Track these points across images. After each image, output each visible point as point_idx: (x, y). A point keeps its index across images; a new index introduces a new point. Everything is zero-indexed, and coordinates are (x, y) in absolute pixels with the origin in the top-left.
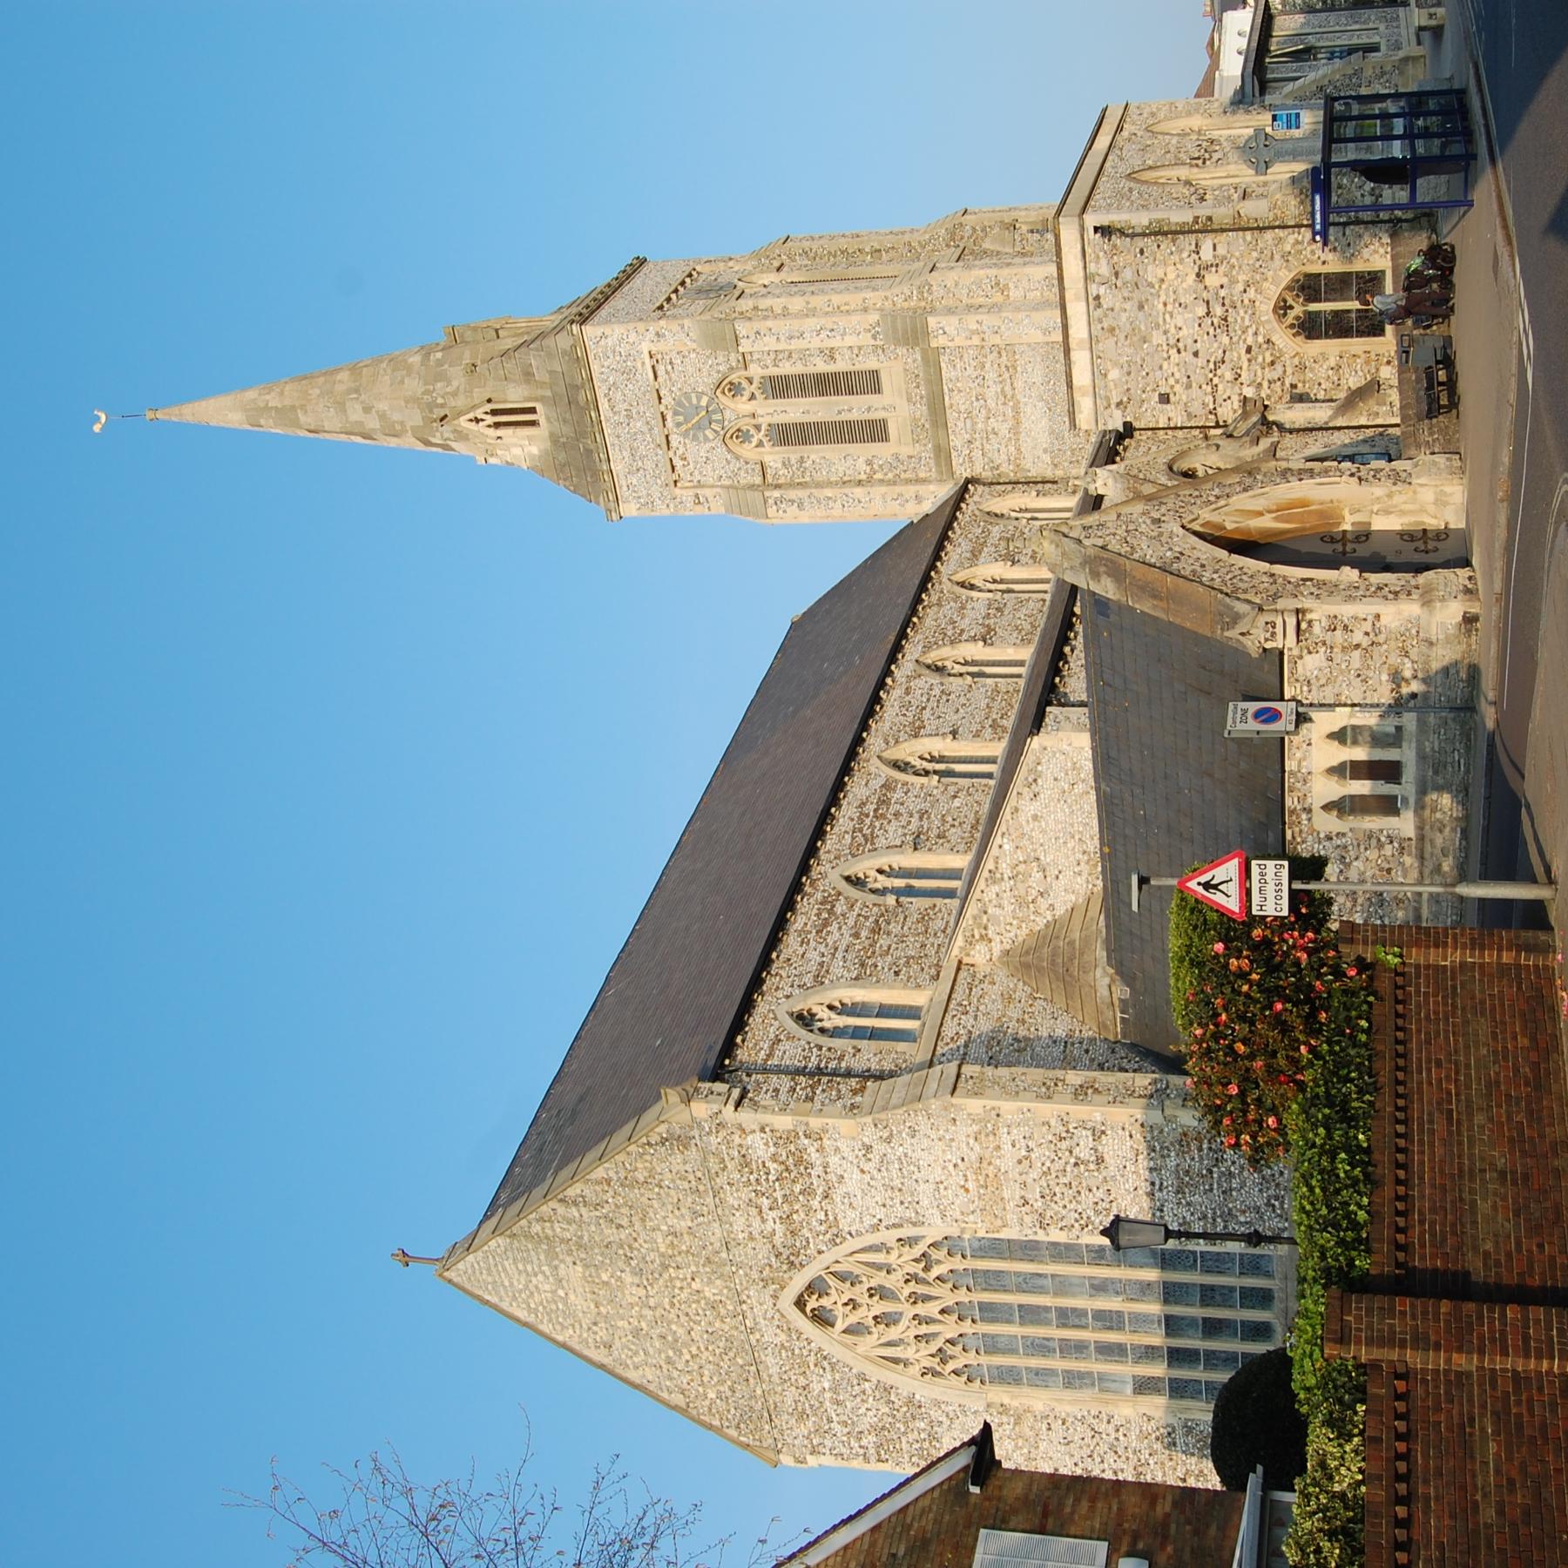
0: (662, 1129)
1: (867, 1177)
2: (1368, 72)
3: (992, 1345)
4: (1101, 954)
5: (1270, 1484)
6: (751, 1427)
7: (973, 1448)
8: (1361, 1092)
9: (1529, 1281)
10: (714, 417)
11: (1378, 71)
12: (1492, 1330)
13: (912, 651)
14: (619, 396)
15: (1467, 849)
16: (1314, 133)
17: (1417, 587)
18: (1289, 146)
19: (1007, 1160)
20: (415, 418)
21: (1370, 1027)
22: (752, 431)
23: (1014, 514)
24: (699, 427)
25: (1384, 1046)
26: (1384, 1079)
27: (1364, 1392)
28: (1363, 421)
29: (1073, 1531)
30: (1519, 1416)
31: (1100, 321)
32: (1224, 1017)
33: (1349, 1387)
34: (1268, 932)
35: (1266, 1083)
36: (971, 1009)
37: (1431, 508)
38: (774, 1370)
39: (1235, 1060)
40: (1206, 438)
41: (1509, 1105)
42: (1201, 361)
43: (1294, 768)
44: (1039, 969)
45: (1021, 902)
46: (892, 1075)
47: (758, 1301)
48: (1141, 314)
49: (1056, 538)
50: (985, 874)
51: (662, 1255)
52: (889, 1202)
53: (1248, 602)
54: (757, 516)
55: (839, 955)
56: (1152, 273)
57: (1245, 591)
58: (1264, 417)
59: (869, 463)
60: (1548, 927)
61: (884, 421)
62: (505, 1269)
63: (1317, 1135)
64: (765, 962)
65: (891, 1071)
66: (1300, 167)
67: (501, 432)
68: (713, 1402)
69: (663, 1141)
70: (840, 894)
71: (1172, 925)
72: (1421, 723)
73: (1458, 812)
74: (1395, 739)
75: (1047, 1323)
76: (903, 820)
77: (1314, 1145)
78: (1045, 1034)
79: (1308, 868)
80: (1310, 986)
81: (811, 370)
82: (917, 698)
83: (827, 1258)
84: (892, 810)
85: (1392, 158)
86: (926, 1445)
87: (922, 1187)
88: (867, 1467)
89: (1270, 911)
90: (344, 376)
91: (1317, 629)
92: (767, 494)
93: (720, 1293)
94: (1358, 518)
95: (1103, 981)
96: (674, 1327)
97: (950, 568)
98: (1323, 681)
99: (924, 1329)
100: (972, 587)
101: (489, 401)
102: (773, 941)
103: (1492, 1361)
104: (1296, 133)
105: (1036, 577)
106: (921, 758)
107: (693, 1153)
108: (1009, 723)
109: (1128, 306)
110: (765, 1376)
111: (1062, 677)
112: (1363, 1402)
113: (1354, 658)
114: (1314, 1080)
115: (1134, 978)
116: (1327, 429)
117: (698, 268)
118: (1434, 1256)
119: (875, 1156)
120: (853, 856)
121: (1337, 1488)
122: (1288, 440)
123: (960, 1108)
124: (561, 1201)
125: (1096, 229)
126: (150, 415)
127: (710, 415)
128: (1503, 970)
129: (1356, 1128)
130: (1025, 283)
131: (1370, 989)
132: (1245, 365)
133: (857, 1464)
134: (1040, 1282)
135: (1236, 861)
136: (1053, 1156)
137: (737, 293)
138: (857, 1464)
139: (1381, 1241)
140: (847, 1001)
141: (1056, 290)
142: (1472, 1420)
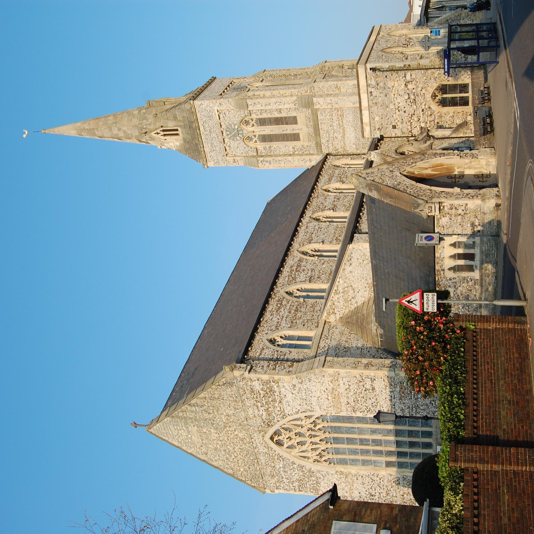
0: (224, 380)
1: (294, 396)
2: (463, 15)
3: (337, 452)
4: (373, 318)
5: (431, 505)
6: (256, 480)
7: (331, 493)
8: (461, 373)
9: (519, 439)
10: (240, 132)
11: (466, 15)
12: (506, 457)
13: (308, 213)
14: (207, 125)
15: (497, 283)
16: (444, 37)
17: (480, 194)
18: (436, 41)
19: (342, 389)
20: (136, 133)
21: (465, 350)
22: (253, 137)
23: (343, 166)
24: (234, 136)
25: (469, 357)
26: (469, 368)
27: (463, 478)
28: (462, 135)
29: (365, 521)
30: (515, 486)
31: (372, 100)
32: (415, 347)
33: (458, 477)
34: (430, 318)
35: (429, 369)
36: (329, 338)
37: (485, 167)
38: (263, 461)
39: (419, 362)
40: (408, 141)
41: (512, 377)
42: (406, 114)
43: (439, 256)
44: (353, 324)
45: (346, 301)
46: (302, 360)
47: (257, 438)
48: (386, 98)
49: (357, 177)
50: (334, 291)
51: (224, 423)
52: (302, 404)
53: (423, 199)
54: (255, 166)
55: (284, 319)
56: (390, 84)
57: (422, 196)
58: (428, 134)
59: (293, 148)
60: (524, 315)
61: (298, 134)
62: (170, 428)
63: (446, 388)
64: (258, 322)
65: (302, 359)
66: (440, 48)
67: (166, 137)
68: (242, 472)
69: (224, 384)
70: (284, 298)
71: (397, 314)
72: (482, 241)
73: (494, 270)
74: (473, 246)
75: (356, 444)
76: (306, 272)
77: (445, 392)
78: (355, 346)
79: (443, 295)
80: (444, 337)
81: (273, 116)
82: (310, 230)
83: (281, 423)
84: (302, 269)
85: (470, 44)
86: (315, 485)
87: (313, 398)
88: (295, 493)
89: (430, 310)
90: (111, 118)
91: (446, 209)
92: (258, 159)
93: (244, 435)
94: (460, 170)
95: (374, 328)
96: (229, 447)
97: (322, 184)
98: (448, 226)
99: (314, 446)
100: (329, 191)
101: (162, 127)
102: (261, 315)
103: (506, 467)
104: (439, 37)
105: (351, 187)
106: (312, 250)
107: (234, 388)
108: (342, 238)
109: (381, 95)
110: (260, 463)
111: (359, 224)
112: (463, 482)
113: (458, 218)
114: (445, 369)
115: (385, 326)
116: (449, 138)
117: (234, 81)
118: (486, 431)
119: (297, 389)
120: (289, 285)
121: (454, 512)
122: (436, 142)
123: (325, 372)
124: (189, 405)
125: (371, 69)
126: (43, 131)
127: (238, 132)
128: (510, 330)
129: (460, 386)
130: (346, 86)
131: (464, 337)
132: (422, 116)
133: (292, 492)
134: (354, 430)
135: (419, 293)
136: (357, 388)
137: (247, 89)
138: (292, 492)
139: (469, 426)
140: (287, 335)
141: (357, 89)
142: (499, 488)
